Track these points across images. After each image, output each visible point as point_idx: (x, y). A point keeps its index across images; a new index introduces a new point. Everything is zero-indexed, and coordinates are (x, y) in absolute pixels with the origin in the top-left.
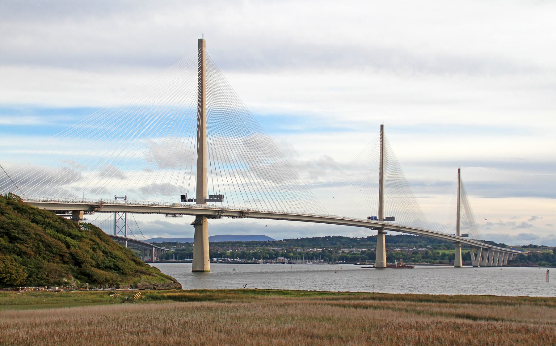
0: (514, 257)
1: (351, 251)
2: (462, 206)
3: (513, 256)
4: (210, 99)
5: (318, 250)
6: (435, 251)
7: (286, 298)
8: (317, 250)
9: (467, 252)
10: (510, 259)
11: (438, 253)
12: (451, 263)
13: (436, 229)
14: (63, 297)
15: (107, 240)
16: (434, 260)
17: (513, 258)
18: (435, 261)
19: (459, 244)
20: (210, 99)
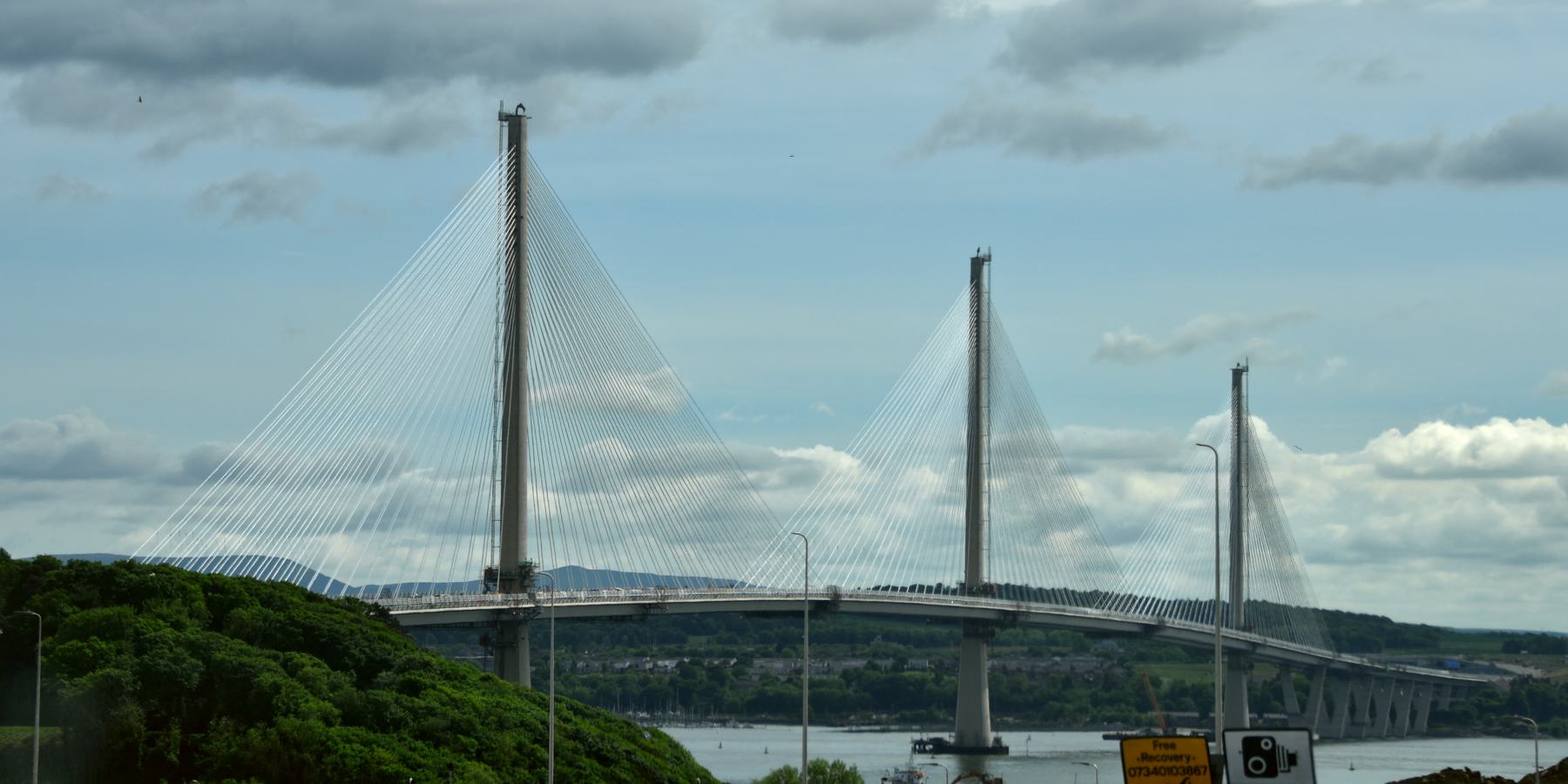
0: (1455, 700)
1: (1468, 660)
2: (1252, 518)
3: (1453, 695)
4: (560, 293)
5: (660, 663)
6: (1140, 668)
7: (498, 439)
8: (655, 665)
9: (1269, 680)
10: (1440, 708)
11: (1156, 683)
12: (1204, 721)
13: (1158, 589)
14: (946, 592)
15: (133, 641)
16: (1139, 712)
17: (1452, 704)
18: (1143, 716)
19: (717, 667)
20: (560, 293)
